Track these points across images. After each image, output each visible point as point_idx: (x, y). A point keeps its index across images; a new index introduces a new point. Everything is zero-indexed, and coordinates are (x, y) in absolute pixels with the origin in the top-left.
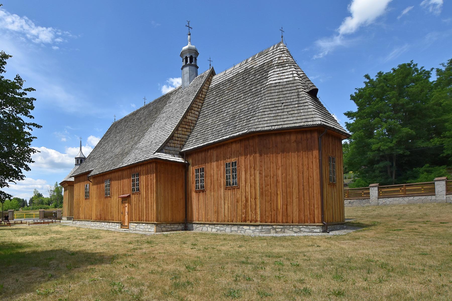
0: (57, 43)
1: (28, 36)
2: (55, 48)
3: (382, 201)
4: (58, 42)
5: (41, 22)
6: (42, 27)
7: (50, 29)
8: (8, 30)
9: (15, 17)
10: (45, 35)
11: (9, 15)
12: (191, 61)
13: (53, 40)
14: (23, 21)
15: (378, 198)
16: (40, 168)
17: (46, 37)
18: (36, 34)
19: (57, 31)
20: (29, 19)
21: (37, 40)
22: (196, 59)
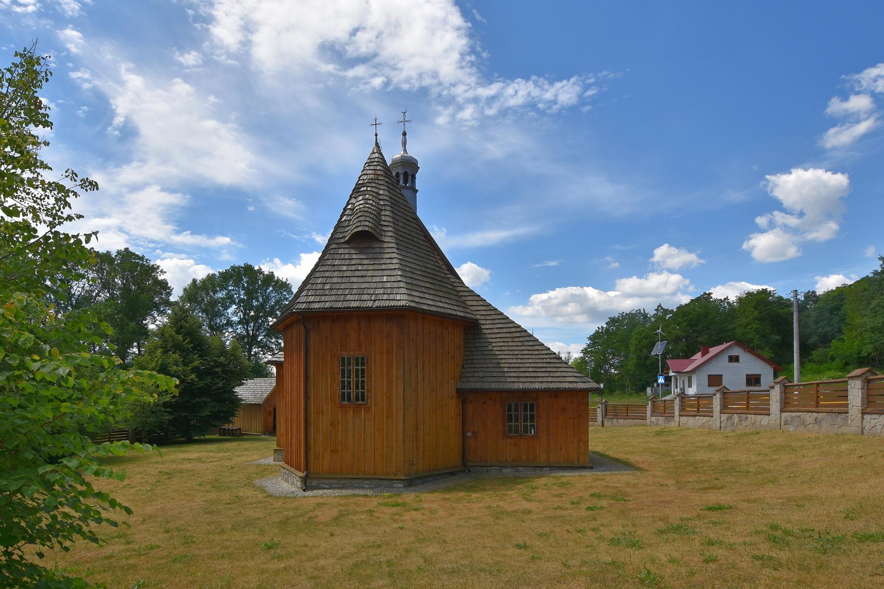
0: (589, 100)
1: (541, 106)
2: (587, 108)
3: (871, 421)
4: (589, 97)
5: (562, 75)
6: (561, 81)
7: (573, 80)
8: (509, 108)
9: (518, 83)
10: (565, 92)
11: (508, 85)
12: (406, 181)
13: (580, 96)
14: (531, 84)
15: (863, 414)
16: (572, 323)
17: (568, 96)
18: (553, 98)
19: (586, 79)
20: (539, 76)
21: (555, 107)
22: (414, 177)
